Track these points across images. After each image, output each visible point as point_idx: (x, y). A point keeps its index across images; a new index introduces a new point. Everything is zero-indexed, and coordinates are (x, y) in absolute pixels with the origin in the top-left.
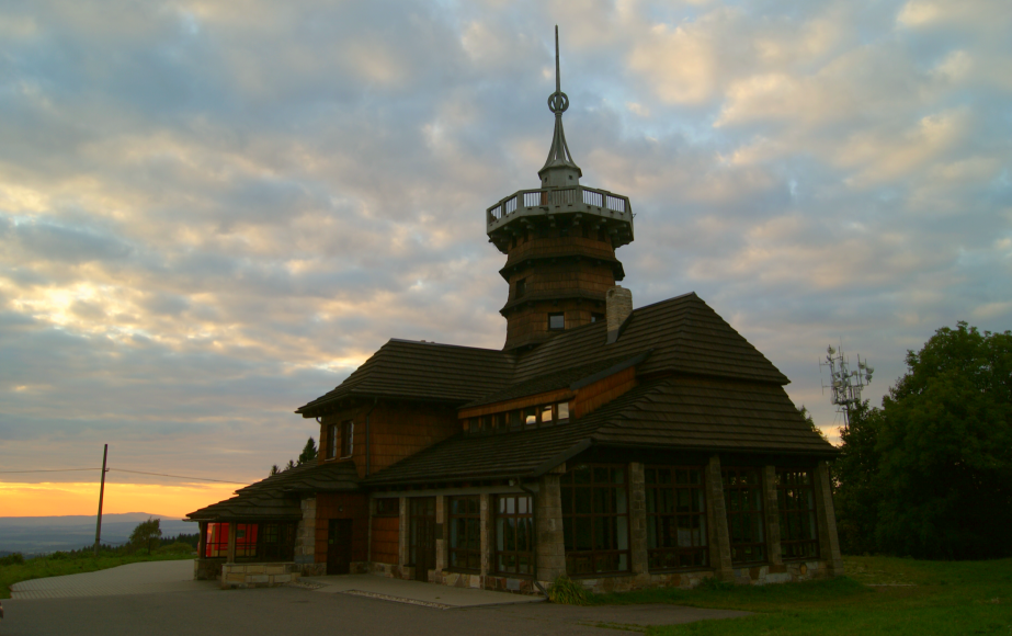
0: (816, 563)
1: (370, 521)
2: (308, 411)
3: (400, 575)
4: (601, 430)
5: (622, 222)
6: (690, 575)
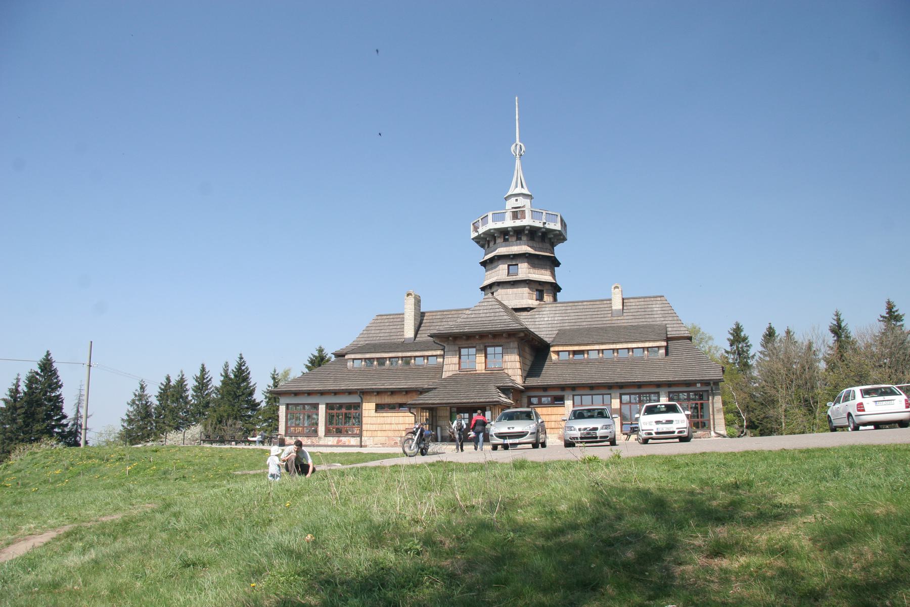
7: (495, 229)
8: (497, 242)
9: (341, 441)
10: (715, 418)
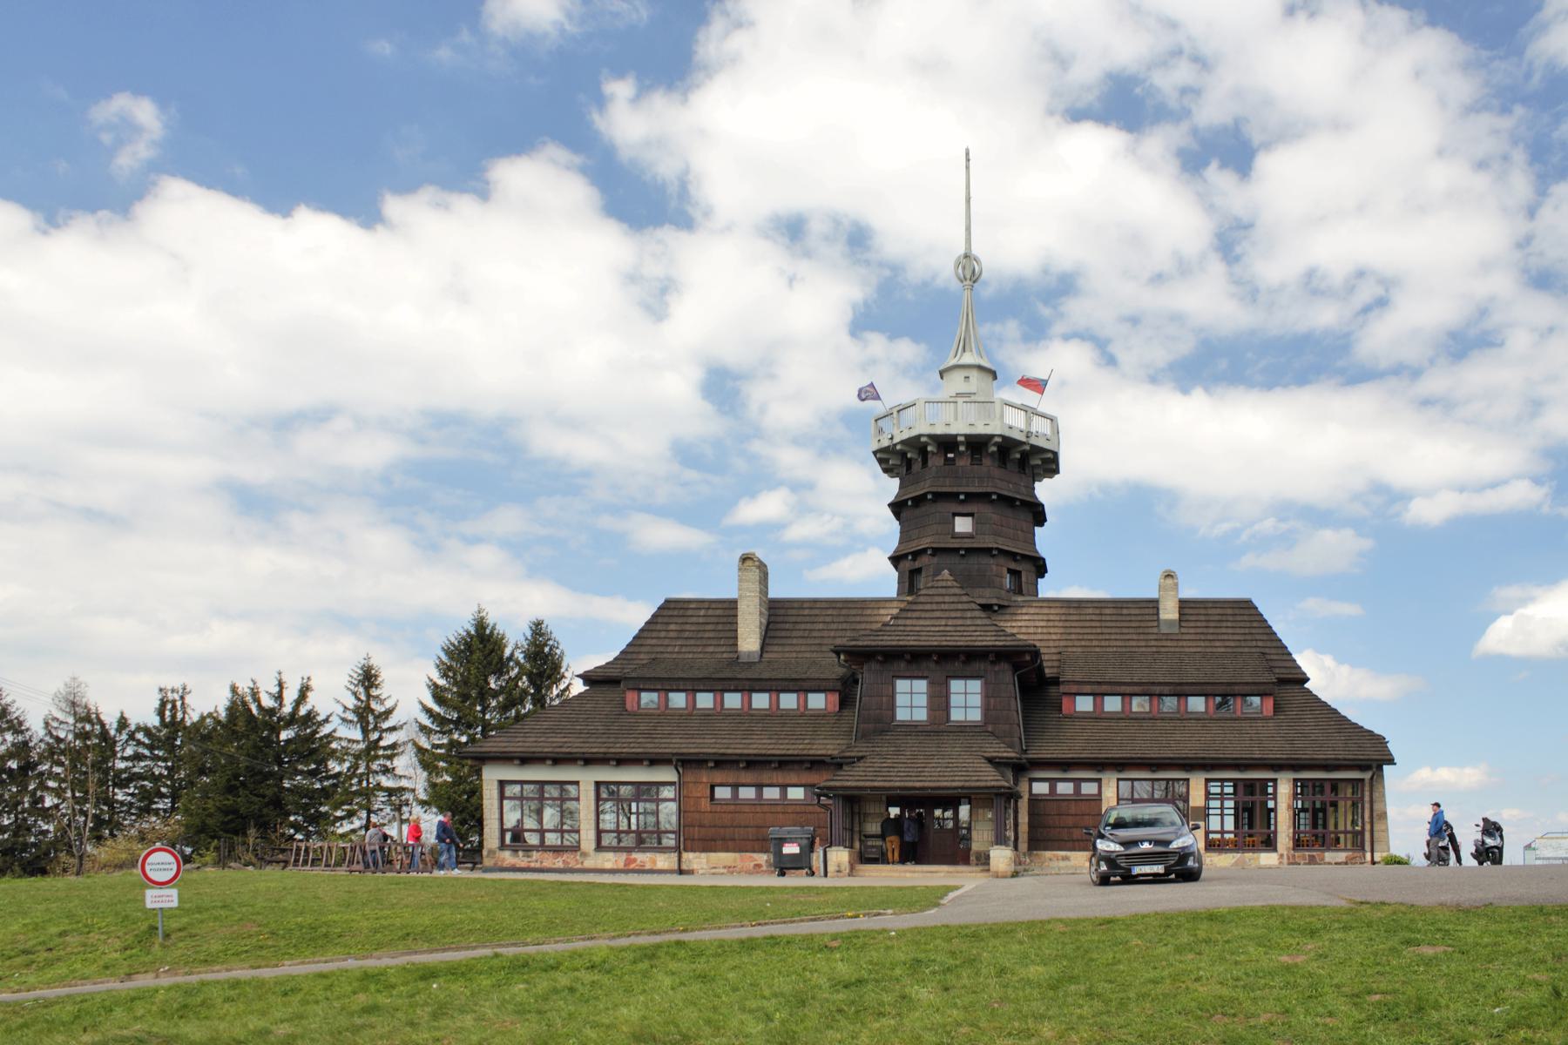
7: (929, 436)
8: (930, 463)
9: (635, 860)
10: (1375, 829)
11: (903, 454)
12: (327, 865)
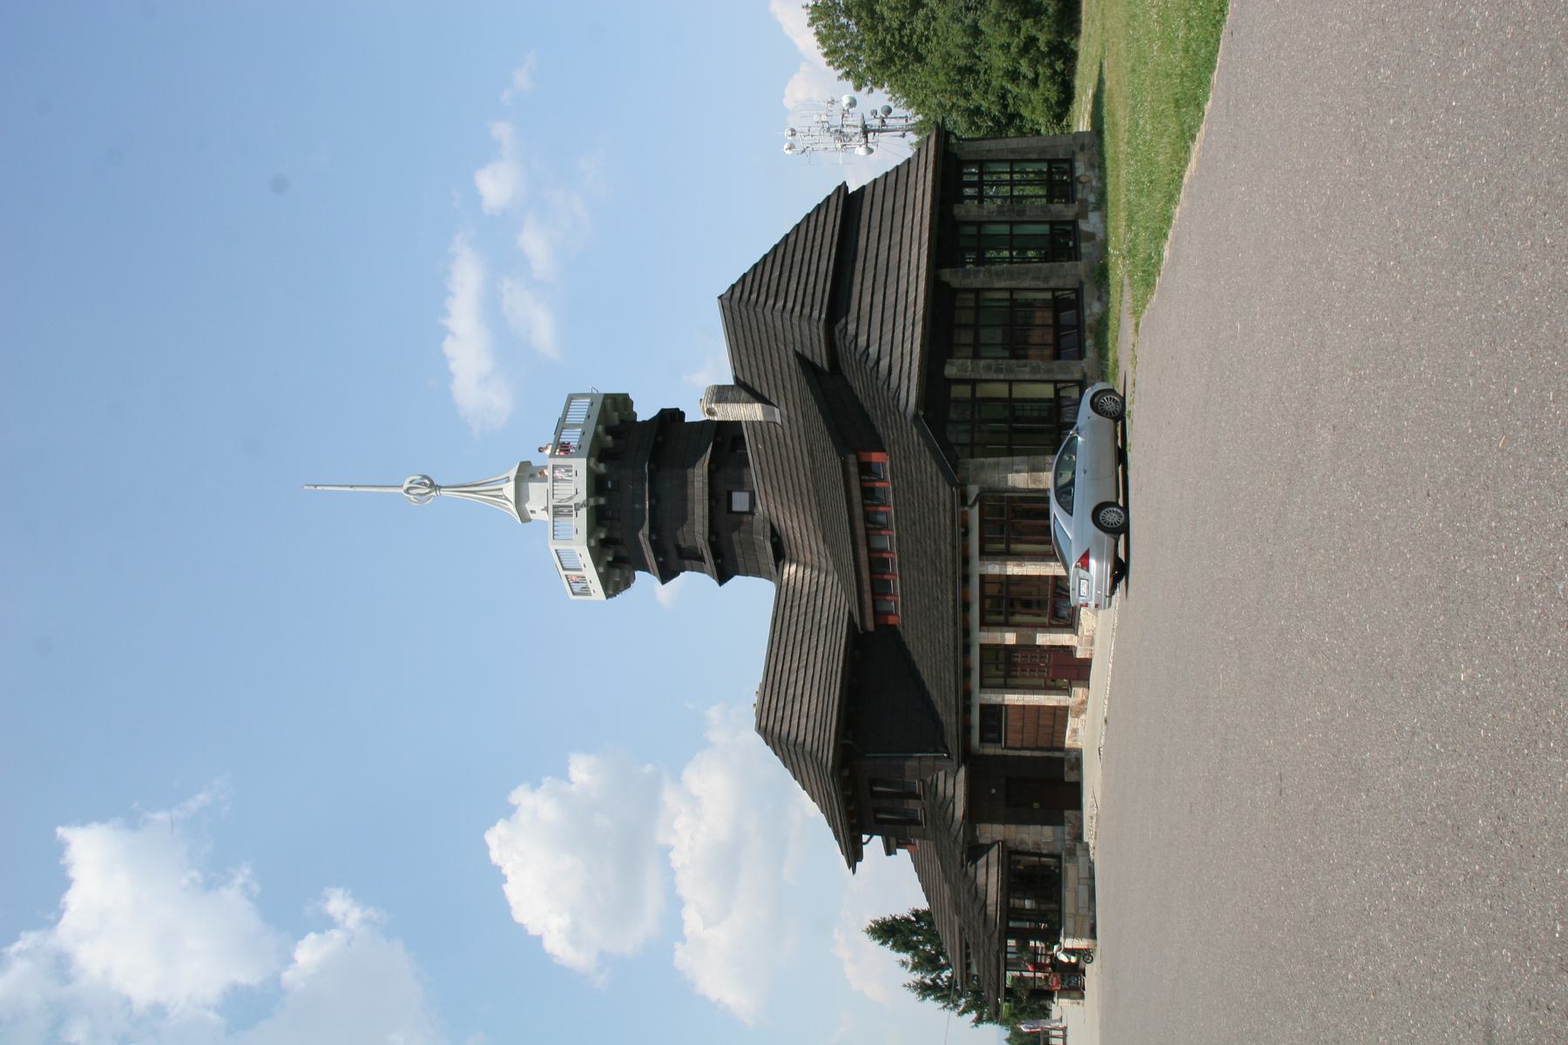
0: (1077, 164)
1: (1010, 753)
2: (854, 855)
3: (1083, 702)
4: (902, 408)
5: (604, 405)
6: (1087, 312)
11: (610, 565)
12: (1105, 608)
